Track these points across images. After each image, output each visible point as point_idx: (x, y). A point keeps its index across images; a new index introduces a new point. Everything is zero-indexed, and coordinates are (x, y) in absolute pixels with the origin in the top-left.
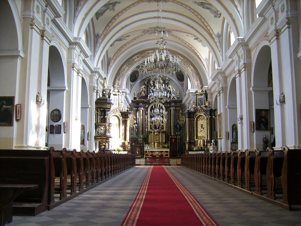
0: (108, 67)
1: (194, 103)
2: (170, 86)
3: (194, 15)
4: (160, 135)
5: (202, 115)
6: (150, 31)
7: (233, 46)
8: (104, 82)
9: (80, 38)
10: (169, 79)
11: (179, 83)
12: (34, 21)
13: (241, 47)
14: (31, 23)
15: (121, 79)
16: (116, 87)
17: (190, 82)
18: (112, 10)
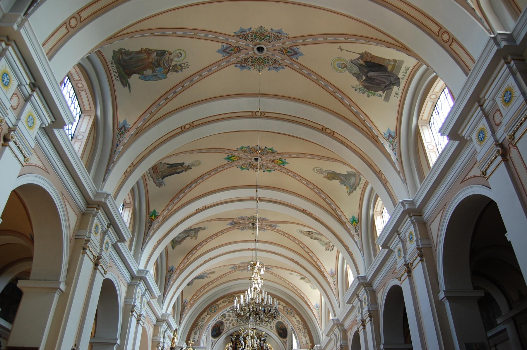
0: (181, 315)
2: (267, 344)
3: (299, 246)
6: (242, 266)
8: (174, 335)
9: (147, 271)
10: (266, 335)
11: (279, 341)
12: (88, 244)
13: (357, 298)
14: (84, 246)
15: (198, 332)
16: (191, 344)
17: (296, 339)
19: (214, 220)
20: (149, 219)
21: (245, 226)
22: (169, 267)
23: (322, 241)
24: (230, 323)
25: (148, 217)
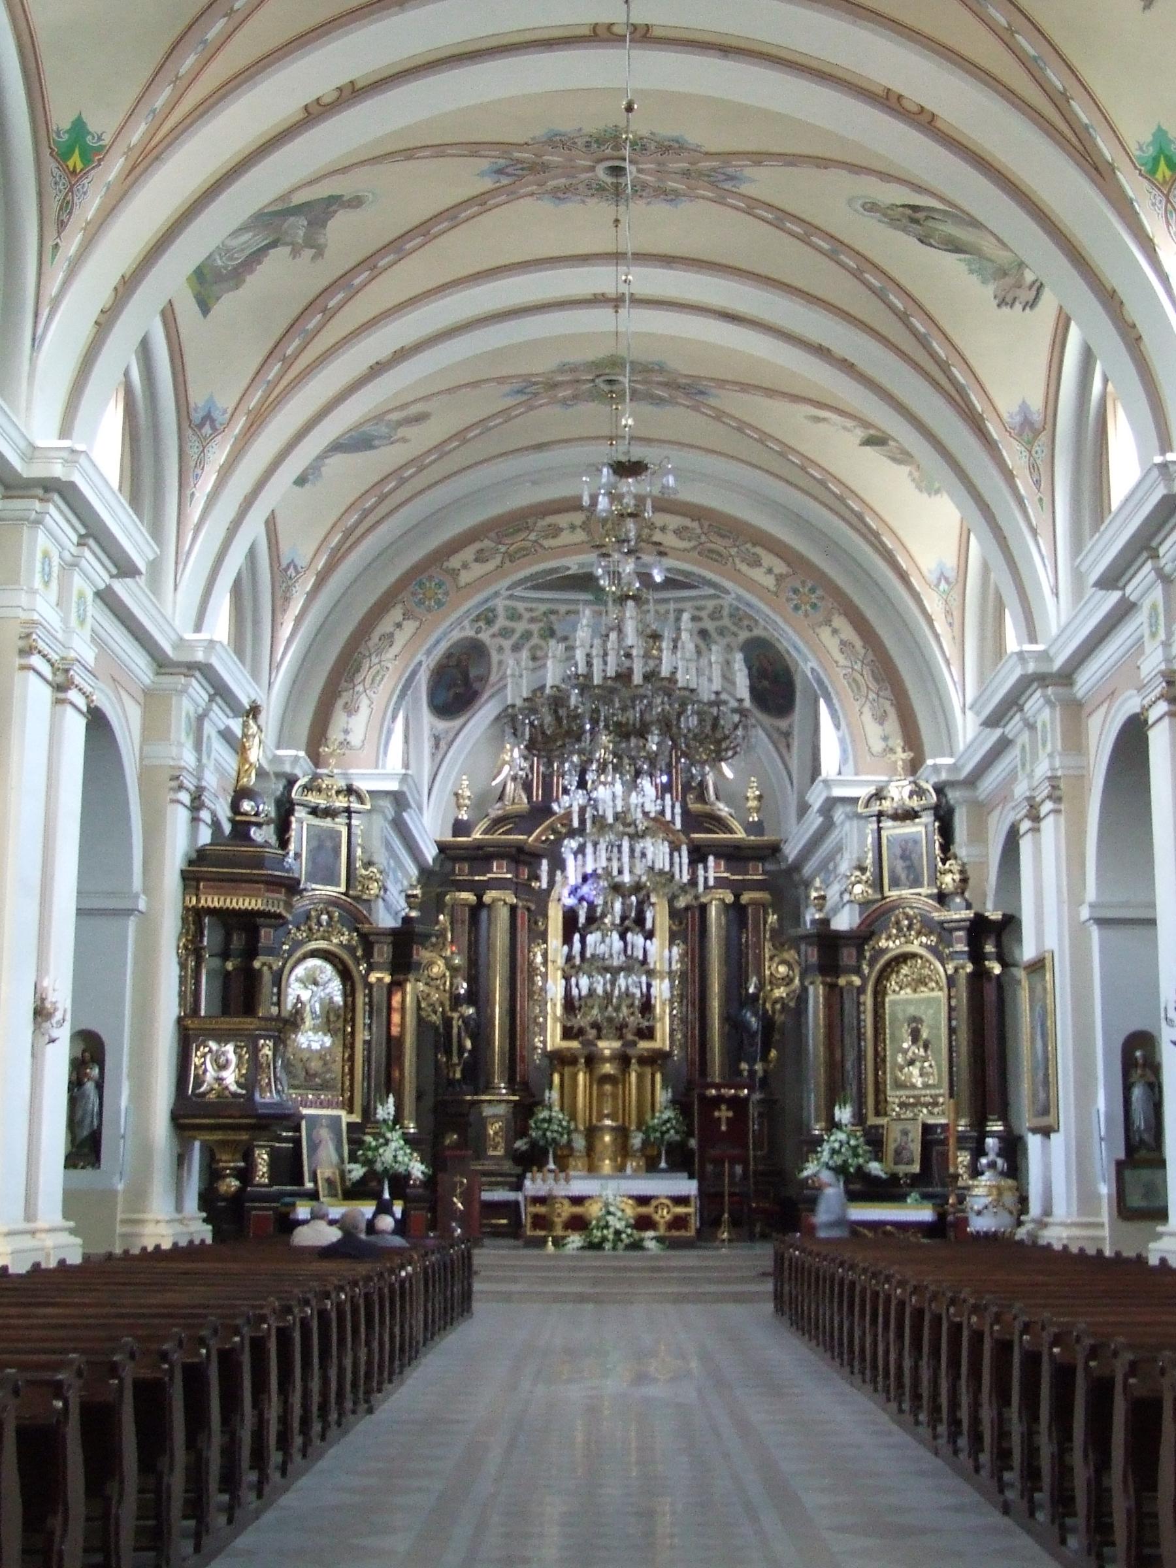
1: (863, 870)
4: (633, 1076)
5: (914, 956)
7: (1125, 512)
17: (838, 726)
18: (308, 253)
19: (409, 154)
20: (56, 172)
21: (574, 181)
22: (192, 405)
23: (980, 257)
24: (516, 648)
25: (51, 160)
